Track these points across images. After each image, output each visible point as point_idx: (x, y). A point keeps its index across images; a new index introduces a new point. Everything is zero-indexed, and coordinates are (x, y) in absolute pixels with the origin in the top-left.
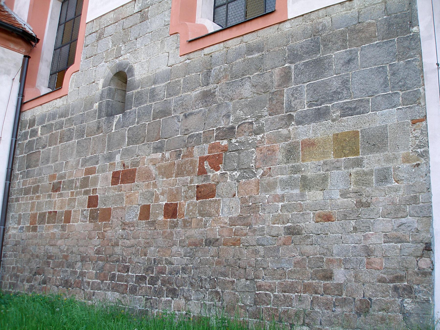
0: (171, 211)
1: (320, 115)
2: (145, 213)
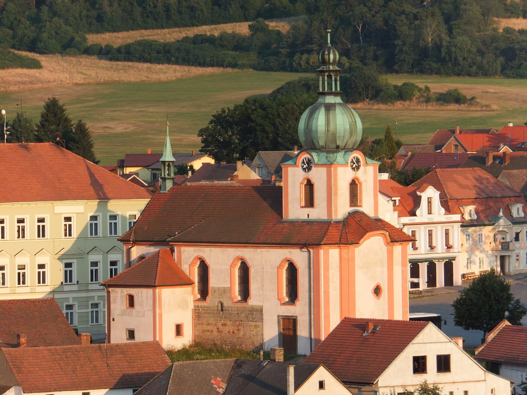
0: (233, 332)
1: (253, 321)
2: (229, 332)
